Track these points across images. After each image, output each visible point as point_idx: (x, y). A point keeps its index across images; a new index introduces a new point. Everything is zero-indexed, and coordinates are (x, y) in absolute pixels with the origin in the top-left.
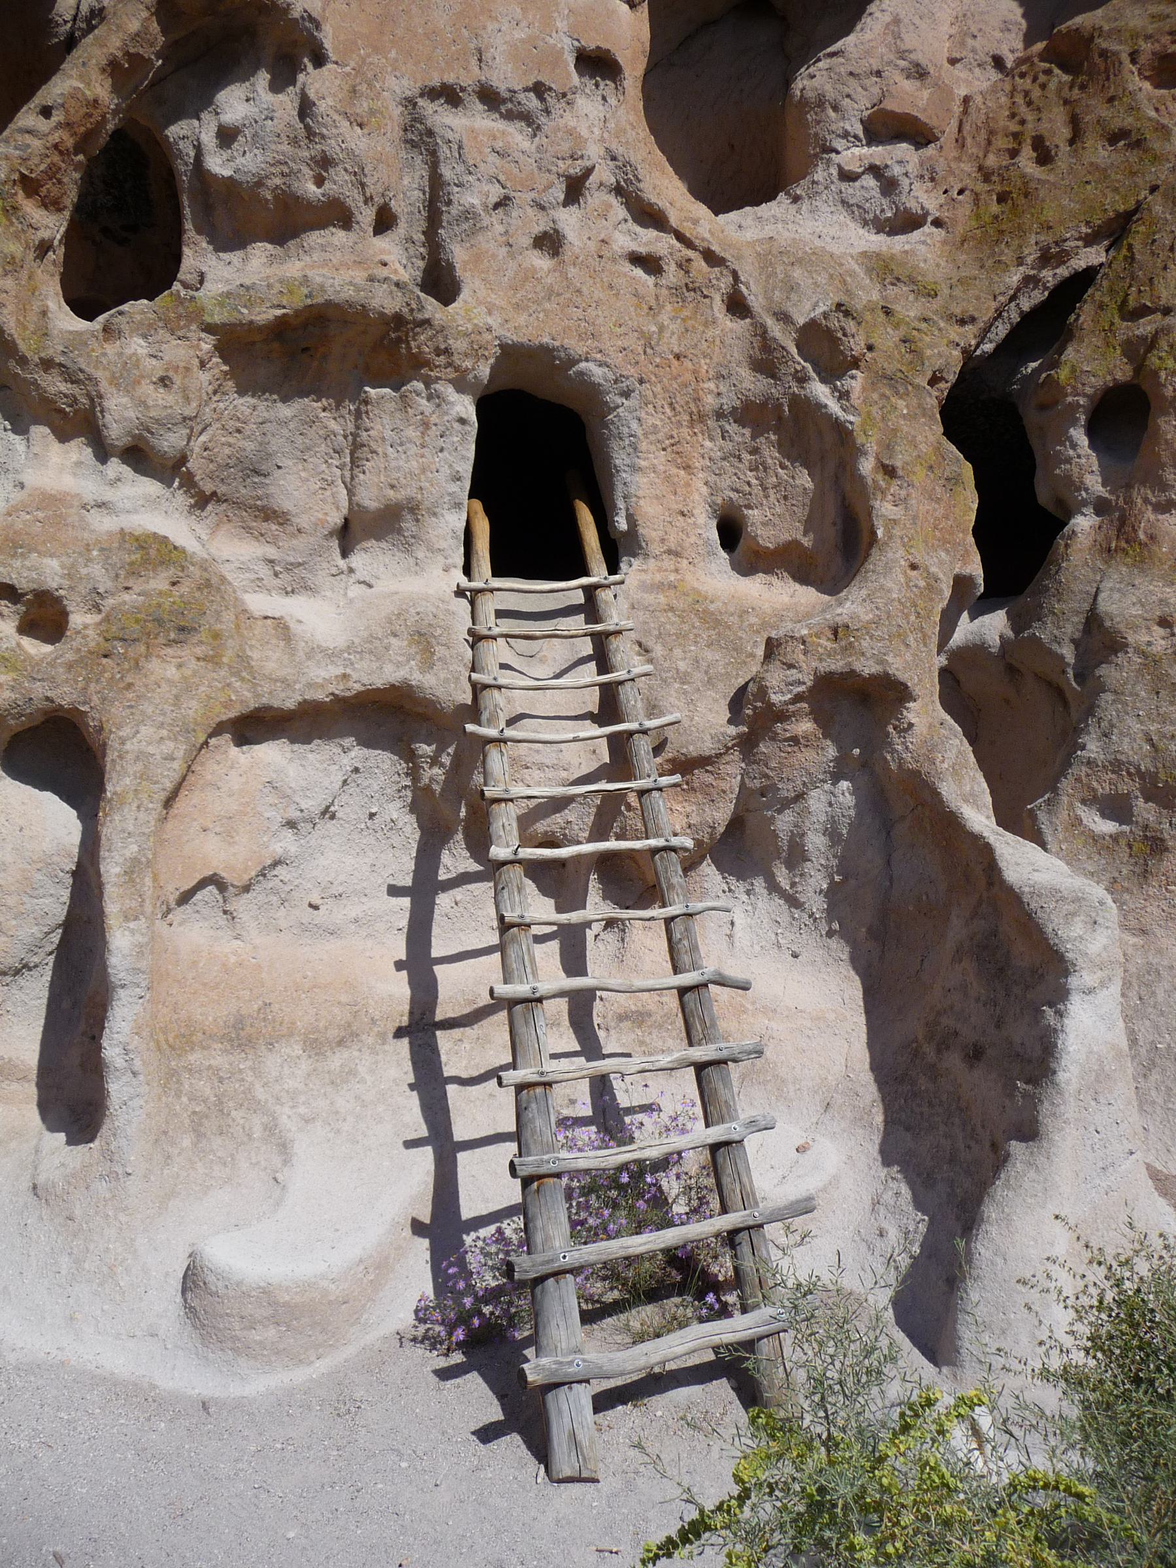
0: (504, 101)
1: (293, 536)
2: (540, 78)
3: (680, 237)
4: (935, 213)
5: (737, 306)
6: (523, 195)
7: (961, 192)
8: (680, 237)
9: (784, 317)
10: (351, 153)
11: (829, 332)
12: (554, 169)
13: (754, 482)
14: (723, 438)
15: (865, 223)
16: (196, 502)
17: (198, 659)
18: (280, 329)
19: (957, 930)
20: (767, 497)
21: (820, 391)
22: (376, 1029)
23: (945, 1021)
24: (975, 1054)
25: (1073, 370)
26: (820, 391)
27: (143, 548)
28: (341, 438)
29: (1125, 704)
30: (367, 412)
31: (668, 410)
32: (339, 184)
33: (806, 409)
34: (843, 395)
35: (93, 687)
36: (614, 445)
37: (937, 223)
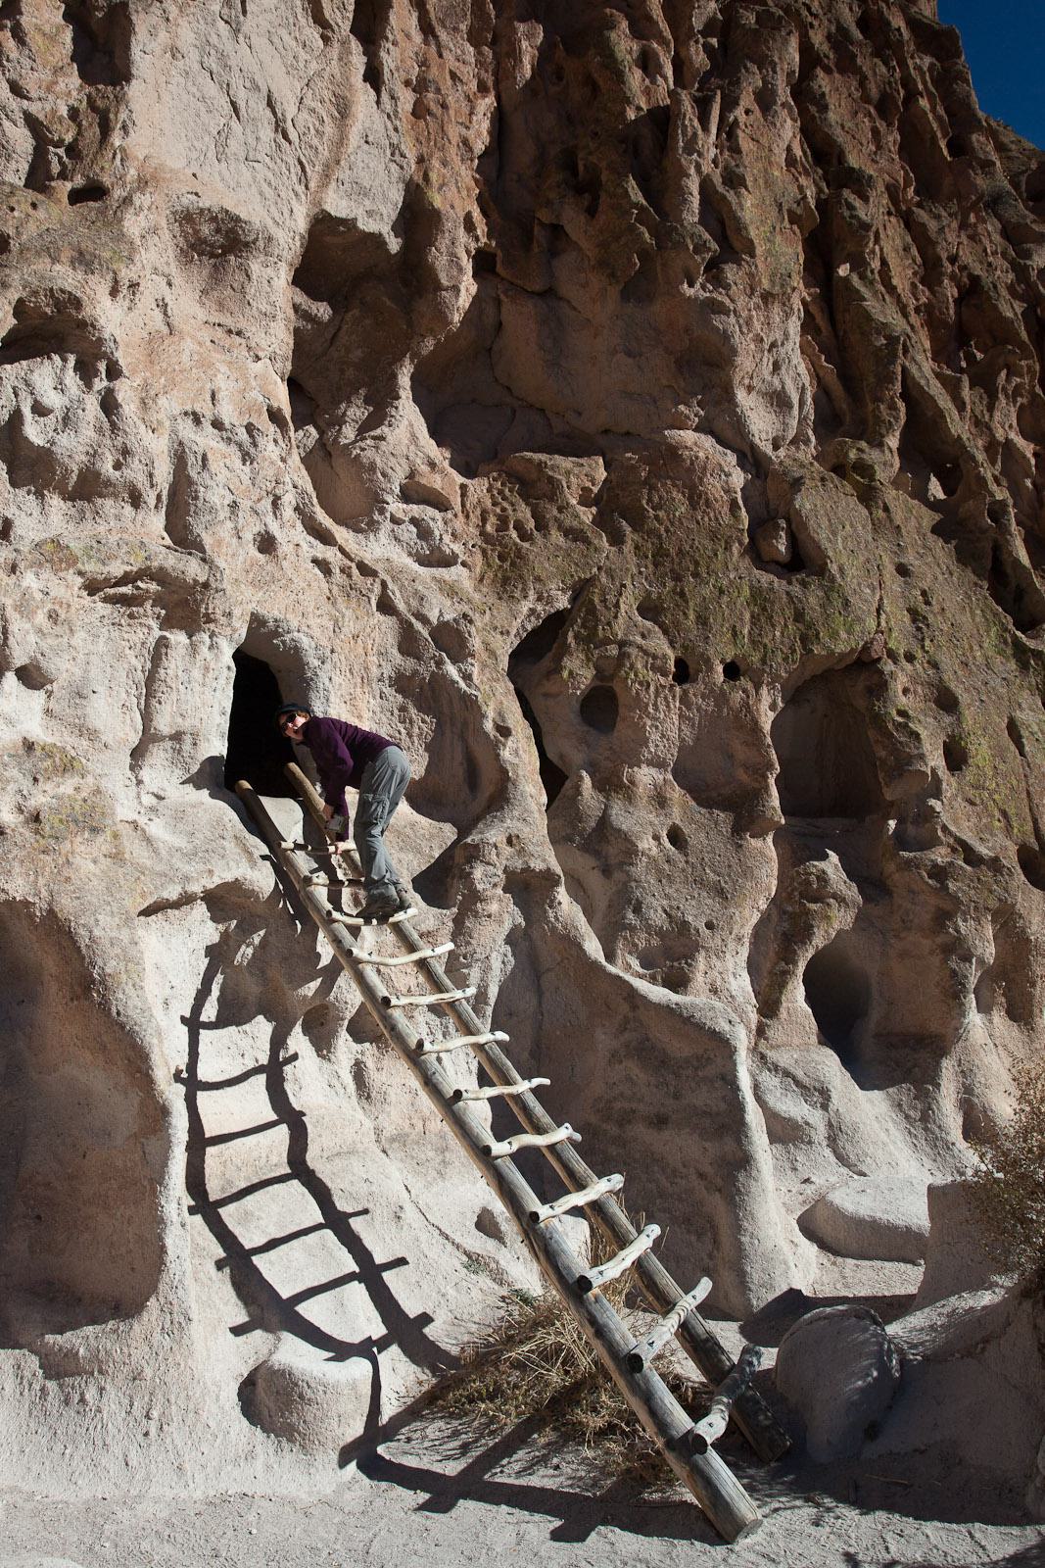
0: (226, 430)
1: (101, 751)
2: (251, 420)
3: (342, 550)
4: (462, 558)
5: (386, 606)
6: (245, 502)
7: (473, 546)
8: (342, 550)
9: (424, 620)
10: (146, 450)
11: (459, 633)
12: (264, 487)
13: (403, 731)
14: (381, 698)
15: (410, 554)
16: (909, 764)
17: (105, 856)
18: (822, 675)
19: (604, 1040)
20: (413, 743)
21: (451, 670)
22: (242, 1175)
23: (618, 1105)
24: (660, 1122)
25: (571, 673)
26: (451, 670)
27: (50, 757)
28: (139, 672)
29: (644, 888)
30: (166, 654)
31: (348, 674)
32: (135, 473)
33: (440, 681)
34: (467, 677)
35: (41, 881)
36: (313, 695)
37: (464, 564)
